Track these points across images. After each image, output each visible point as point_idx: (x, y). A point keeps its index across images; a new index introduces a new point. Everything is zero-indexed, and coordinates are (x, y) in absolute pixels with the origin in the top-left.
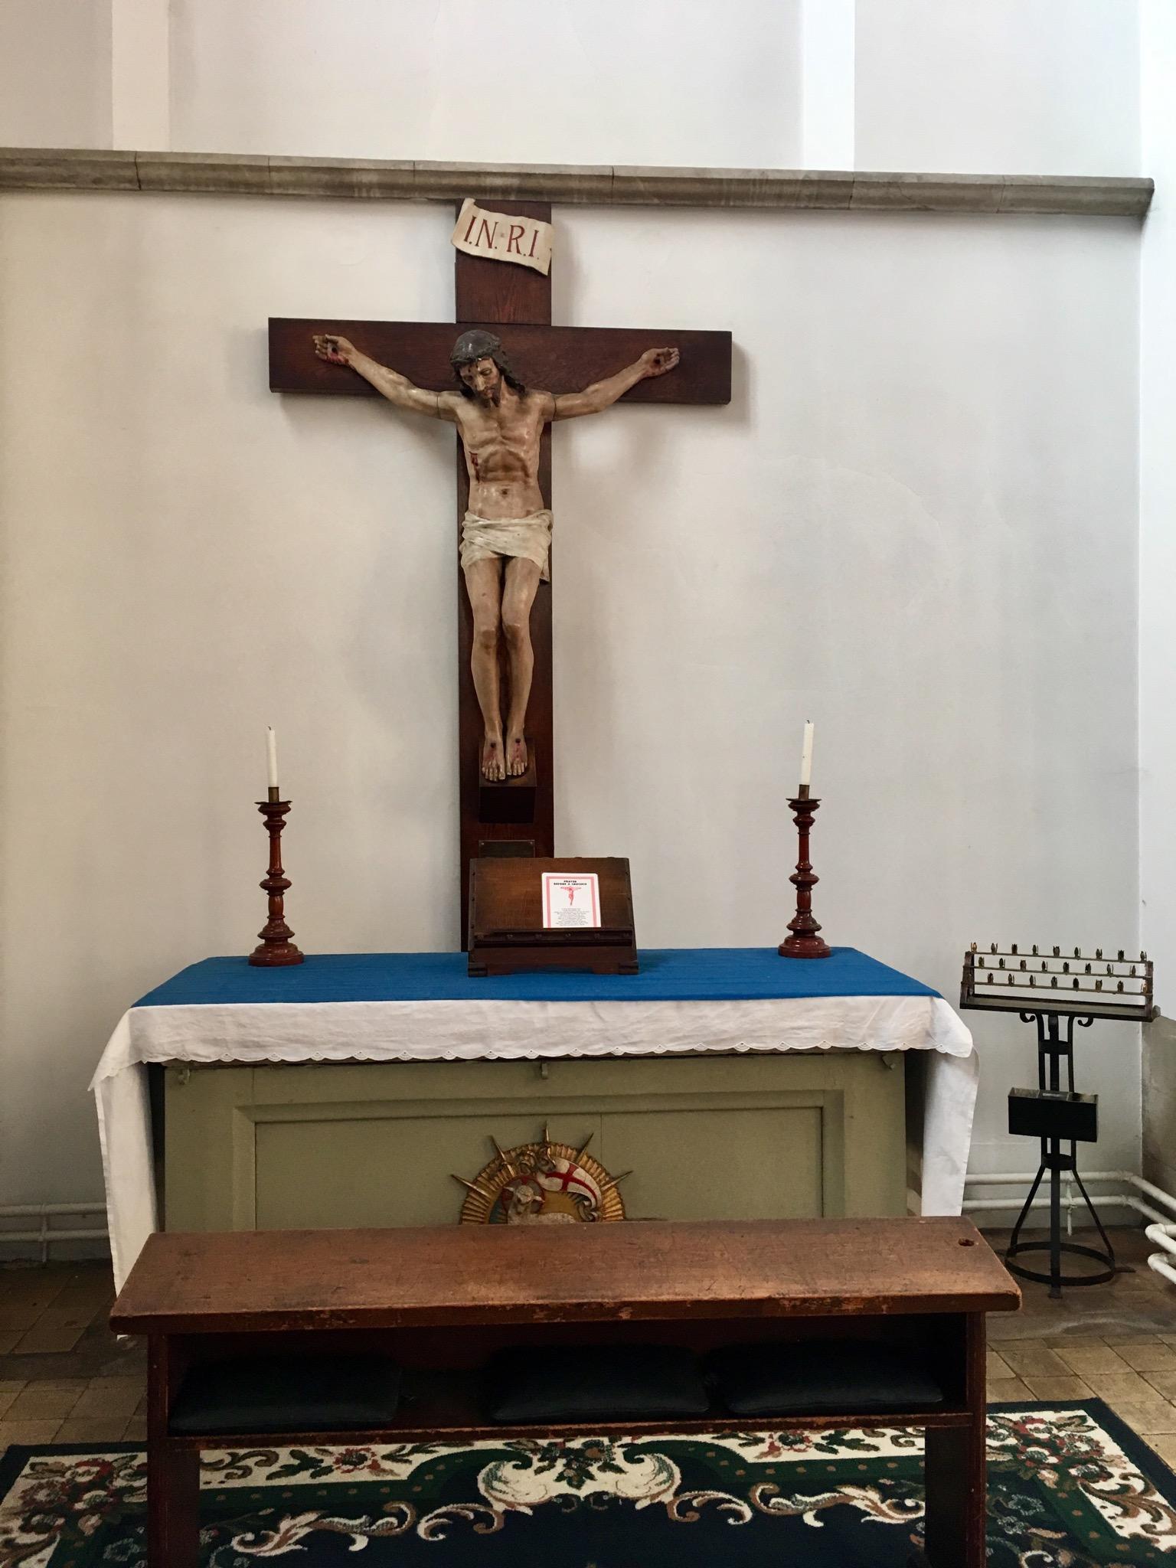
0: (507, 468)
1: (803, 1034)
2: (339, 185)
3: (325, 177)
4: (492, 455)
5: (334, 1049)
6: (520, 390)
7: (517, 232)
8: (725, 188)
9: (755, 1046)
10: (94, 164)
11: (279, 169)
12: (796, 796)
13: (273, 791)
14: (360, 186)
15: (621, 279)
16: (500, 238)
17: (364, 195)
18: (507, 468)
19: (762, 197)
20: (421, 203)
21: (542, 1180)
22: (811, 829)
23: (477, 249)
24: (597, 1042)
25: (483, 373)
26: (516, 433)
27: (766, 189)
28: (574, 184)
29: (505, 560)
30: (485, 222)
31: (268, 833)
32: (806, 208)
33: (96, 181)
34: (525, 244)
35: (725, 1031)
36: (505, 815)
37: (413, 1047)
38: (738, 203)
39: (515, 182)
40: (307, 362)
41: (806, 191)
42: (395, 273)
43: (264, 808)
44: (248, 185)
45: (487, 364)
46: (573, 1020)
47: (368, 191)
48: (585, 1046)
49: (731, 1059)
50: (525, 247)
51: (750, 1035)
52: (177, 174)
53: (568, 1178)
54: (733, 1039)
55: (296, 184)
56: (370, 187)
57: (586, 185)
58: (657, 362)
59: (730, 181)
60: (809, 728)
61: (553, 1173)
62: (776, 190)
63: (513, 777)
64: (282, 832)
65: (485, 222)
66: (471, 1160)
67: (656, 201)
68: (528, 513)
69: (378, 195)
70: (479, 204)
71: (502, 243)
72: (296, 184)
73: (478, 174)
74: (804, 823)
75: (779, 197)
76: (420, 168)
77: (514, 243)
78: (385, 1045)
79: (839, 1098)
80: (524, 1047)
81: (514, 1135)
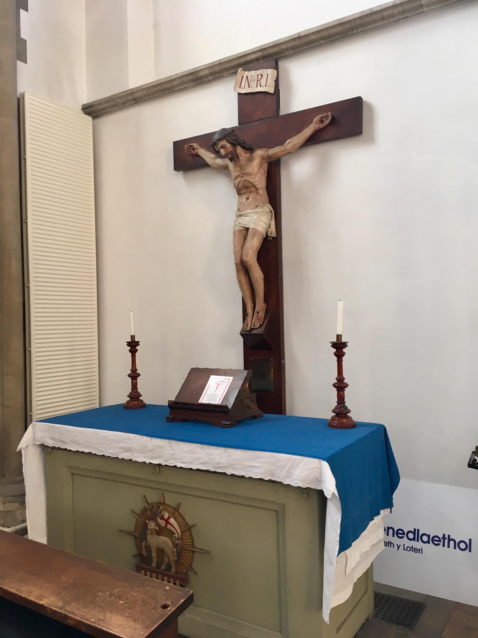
0: (247, 188)
1: (256, 470)
2: (197, 79)
3: (190, 77)
4: (239, 182)
5: (85, 448)
6: (250, 150)
7: (260, 76)
8: (353, 24)
9: (234, 473)
10: (121, 97)
11: (175, 79)
12: (335, 340)
13: (133, 337)
14: (203, 77)
15: (311, 85)
16: (261, 81)
17: (206, 80)
18: (247, 188)
19: (374, 22)
20: (227, 77)
21: (159, 520)
22: (344, 358)
23: (243, 91)
24: (171, 460)
25: (222, 147)
26: (247, 171)
27: (374, 17)
28: (284, 47)
29: (247, 229)
30: (247, 77)
31: (131, 354)
32: (399, 20)
33: (124, 103)
34: (263, 82)
35: (220, 463)
36: (264, 347)
37: (109, 451)
38: (363, 29)
39: (259, 54)
40: (187, 157)
41: (396, 11)
42: (215, 110)
43: (129, 344)
44: (167, 89)
45: (224, 143)
46: (162, 447)
47: (207, 78)
48: (166, 461)
49: (223, 476)
50: (263, 84)
51: (230, 466)
52: (145, 92)
53: (167, 521)
54: (224, 467)
55: (182, 84)
56: (207, 76)
57: (289, 45)
58: (322, 121)
59: (355, 19)
60: (132, 314)
61: (162, 518)
62: (379, 15)
63: (254, 329)
64: (136, 354)
65: (247, 77)
66: (139, 506)
67: (323, 42)
68: (257, 206)
69: (211, 78)
70: (244, 70)
71: (253, 84)
72: (182, 84)
73: (244, 56)
74: (339, 355)
75: (383, 18)
76: (222, 61)
77: (259, 82)
78: (101, 449)
79: (283, 506)
80: (145, 457)
81: (153, 497)
